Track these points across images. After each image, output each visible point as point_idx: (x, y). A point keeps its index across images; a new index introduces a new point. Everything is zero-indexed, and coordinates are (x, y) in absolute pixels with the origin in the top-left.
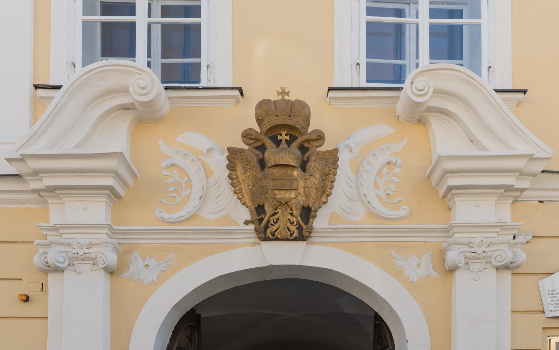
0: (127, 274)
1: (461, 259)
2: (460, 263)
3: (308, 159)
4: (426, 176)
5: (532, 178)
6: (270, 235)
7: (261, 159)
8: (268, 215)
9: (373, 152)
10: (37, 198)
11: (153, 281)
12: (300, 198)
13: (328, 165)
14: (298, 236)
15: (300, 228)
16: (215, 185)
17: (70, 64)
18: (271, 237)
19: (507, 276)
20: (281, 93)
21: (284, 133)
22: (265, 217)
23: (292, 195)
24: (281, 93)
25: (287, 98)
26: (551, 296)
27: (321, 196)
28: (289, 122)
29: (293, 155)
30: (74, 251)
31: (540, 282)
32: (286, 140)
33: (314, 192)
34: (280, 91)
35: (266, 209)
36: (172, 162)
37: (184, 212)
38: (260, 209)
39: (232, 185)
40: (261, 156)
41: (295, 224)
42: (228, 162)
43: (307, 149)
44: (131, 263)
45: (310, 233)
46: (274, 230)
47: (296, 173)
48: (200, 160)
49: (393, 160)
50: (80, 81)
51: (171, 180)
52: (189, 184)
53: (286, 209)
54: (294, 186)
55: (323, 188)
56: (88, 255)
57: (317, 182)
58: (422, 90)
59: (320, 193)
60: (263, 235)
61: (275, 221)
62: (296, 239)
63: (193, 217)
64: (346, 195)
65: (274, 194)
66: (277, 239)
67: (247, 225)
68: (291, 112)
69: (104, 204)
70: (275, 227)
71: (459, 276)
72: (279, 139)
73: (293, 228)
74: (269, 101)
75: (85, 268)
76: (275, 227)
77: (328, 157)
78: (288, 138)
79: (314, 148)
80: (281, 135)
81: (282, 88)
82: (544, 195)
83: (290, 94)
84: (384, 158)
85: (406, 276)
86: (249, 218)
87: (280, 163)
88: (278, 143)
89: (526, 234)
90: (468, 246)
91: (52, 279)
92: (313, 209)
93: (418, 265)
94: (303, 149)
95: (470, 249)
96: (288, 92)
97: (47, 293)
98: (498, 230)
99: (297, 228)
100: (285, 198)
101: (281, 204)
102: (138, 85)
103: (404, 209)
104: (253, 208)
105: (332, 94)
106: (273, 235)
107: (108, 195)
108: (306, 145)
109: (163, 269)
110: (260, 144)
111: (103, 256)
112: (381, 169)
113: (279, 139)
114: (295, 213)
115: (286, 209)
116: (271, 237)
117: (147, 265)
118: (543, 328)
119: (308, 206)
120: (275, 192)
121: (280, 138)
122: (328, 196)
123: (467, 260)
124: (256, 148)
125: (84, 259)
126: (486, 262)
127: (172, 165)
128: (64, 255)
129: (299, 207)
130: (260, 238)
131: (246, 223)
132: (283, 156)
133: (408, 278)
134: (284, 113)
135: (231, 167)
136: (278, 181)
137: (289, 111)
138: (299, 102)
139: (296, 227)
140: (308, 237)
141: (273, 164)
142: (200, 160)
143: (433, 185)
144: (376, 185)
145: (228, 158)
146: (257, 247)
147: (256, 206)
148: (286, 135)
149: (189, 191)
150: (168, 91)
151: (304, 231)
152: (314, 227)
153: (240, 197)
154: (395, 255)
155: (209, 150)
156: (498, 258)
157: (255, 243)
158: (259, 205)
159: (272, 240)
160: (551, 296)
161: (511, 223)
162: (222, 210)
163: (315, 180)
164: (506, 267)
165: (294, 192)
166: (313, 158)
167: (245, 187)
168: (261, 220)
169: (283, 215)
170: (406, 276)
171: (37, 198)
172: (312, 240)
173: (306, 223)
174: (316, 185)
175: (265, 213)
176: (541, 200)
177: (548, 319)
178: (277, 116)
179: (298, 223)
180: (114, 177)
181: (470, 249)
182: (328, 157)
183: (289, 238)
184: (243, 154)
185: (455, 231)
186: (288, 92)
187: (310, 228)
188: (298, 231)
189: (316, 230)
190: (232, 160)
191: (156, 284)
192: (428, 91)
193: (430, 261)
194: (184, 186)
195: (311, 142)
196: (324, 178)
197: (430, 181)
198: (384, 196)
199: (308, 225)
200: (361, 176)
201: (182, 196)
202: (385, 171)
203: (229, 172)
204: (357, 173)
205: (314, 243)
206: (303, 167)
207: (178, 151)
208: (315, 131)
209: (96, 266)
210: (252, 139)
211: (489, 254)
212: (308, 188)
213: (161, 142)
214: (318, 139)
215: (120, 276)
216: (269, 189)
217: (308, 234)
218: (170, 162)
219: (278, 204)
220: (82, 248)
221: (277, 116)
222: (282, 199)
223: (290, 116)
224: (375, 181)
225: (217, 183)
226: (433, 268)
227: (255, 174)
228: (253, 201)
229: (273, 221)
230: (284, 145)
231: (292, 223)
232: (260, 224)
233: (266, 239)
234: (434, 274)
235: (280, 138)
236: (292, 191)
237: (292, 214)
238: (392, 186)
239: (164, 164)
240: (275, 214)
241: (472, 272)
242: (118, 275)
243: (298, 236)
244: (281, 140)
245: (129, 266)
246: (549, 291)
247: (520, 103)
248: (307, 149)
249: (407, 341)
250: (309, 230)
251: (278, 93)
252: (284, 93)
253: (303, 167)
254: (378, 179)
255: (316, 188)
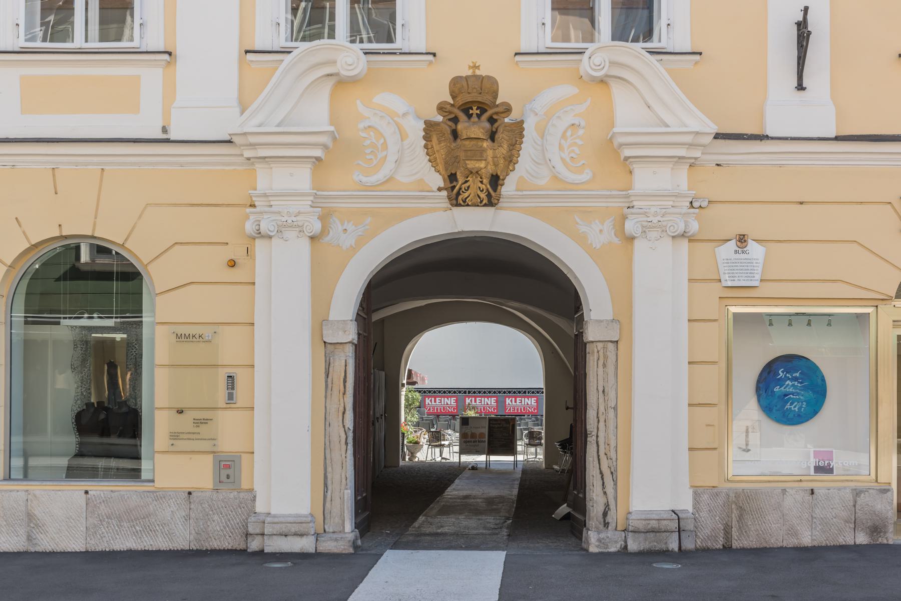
0: (327, 239)
1: (638, 229)
2: (636, 233)
3: (497, 129)
4: (608, 138)
5: (703, 148)
6: (461, 202)
7: (454, 129)
8: (460, 183)
9: (557, 115)
10: (244, 161)
11: (351, 246)
12: (489, 167)
13: (515, 135)
14: (487, 203)
15: (489, 196)
16: (409, 148)
17: (274, 23)
18: (463, 204)
19: (685, 244)
20: (472, 67)
21: (475, 108)
22: (457, 185)
23: (482, 165)
24: (472, 67)
25: (478, 72)
26: (725, 265)
27: (509, 165)
28: (479, 99)
29: (483, 130)
30: (284, 219)
31: (716, 249)
32: (477, 114)
33: (502, 161)
34: (471, 65)
35: (458, 177)
36: (370, 124)
37: (380, 176)
38: (452, 177)
39: (427, 154)
40: (454, 127)
41: (484, 191)
42: (424, 134)
43: (496, 121)
44: (330, 227)
45: (498, 200)
46: (465, 197)
47: (485, 144)
48: (395, 121)
49: (577, 123)
50: (295, 60)
51: (368, 142)
52: (385, 146)
53: (476, 177)
54: (483, 157)
55: (510, 158)
56: (295, 223)
57: (505, 152)
58: (599, 65)
59: (507, 163)
60: (454, 202)
61: (466, 188)
62: (485, 205)
63: (390, 180)
64: (533, 159)
65: (466, 164)
66: (468, 205)
67: (440, 191)
68: (481, 90)
69: (309, 170)
70: (466, 195)
71: (637, 243)
72: (470, 113)
73: (483, 195)
74: (461, 77)
75: (291, 234)
76: (466, 195)
77: (514, 128)
78: (478, 112)
79: (502, 119)
80: (472, 109)
81: (473, 62)
82: (721, 159)
83: (480, 67)
84: (568, 119)
85: (589, 242)
86: (442, 185)
87: (471, 137)
88: (470, 116)
89: (702, 200)
90: (644, 216)
91: (259, 243)
92: (501, 177)
93: (601, 231)
94: (492, 120)
95: (646, 219)
96: (479, 66)
97: (253, 259)
98: (673, 198)
99: (486, 195)
100: (475, 168)
101: (471, 173)
102: (346, 62)
103: (587, 173)
104: (446, 177)
105: (518, 58)
106: (464, 201)
107: (314, 162)
108: (495, 117)
109: (360, 233)
110: (452, 116)
111: (311, 226)
112: (565, 132)
113: (470, 113)
114: (485, 181)
115: (476, 177)
116: (463, 204)
117: (346, 229)
118: (720, 298)
119: (497, 175)
120: (467, 162)
121: (471, 112)
122: (515, 164)
123: (644, 229)
124: (450, 120)
125: (291, 227)
126: (663, 231)
127: (369, 127)
128: (274, 223)
129: (489, 175)
130: (452, 205)
131: (440, 189)
132: (474, 131)
133: (591, 244)
134: (475, 90)
135: (427, 138)
136: (469, 152)
137: (479, 89)
138: (489, 77)
139: (486, 194)
140: (496, 204)
141: (465, 138)
142: (395, 121)
143: (615, 147)
144: (561, 148)
145: (425, 130)
146: (449, 212)
147: (449, 174)
148: (477, 109)
149: (385, 153)
150: (367, 55)
151: (493, 198)
152: (502, 194)
153: (434, 166)
154: (578, 220)
155: (404, 115)
156: (672, 228)
157: (447, 208)
158: (451, 173)
159: (463, 206)
160: (725, 265)
161: (688, 191)
162: (416, 173)
163: (503, 150)
164: (683, 235)
165: (484, 162)
166: (501, 130)
167: (441, 155)
168: (453, 188)
169: (474, 183)
170: (589, 242)
171: (244, 161)
172: (500, 205)
173: (495, 190)
174: (504, 155)
175: (457, 180)
176: (718, 163)
177: (726, 289)
178: (469, 93)
179: (488, 190)
180: (322, 148)
181: (646, 219)
182: (514, 128)
183: (479, 204)
184: (439, 127)
185: (633, 199)
186: (479, 66)
187: (498, 196)
188: (487, 199)
189: (504, 196)
190: (428, 132)
191: (354, 249)
192: (605, 65)
193: (612, 226)
194: (380, 149)
195: (499, 114)
196: (511, 148)
197: (612, 143)
198: (568, 160)
199: (496, 193)
200: (547, 140)
201: (379, 159)
202: (569, 133)
203: (425, 142)
204: (542, 137)
205: (501, 209)
206: (492, 137)
207: (375, 113)
208: (503, 104)
209: (302, 233)
210: (446, 112)
211: (664, 224)
212: (496, 157)
213: (358, 102)
214: (505, 112)
215: (320, 241)
216: (461, 159)
217: (496, 202)
218: (367, 124)
219: (469, 173)
220: (290, 216)
221: (469, 93)
222: (473, 168)
223: (480, 93)
224: (560, 144)
225: (411, 146)
226: (615, 235)
227: (448, 145)
228: (446, 170)
229: (465, 188)
230: (474, 118)
231: (482, 191)
232: (452, 190)
233: (458, 205)
234: (616, 240)
235: (471, 112)
236: (483, 161)
237: (482, 182)
238: (575, 148)
239: (361, 126)
240: (466, 182)
241: (650, 240)
242: (319, 240)
243: (487, 203)
244: (472, 114)
245: (329, 230)
246: (724, 260)
247: (696, 63)
248: (496, 121)
249: (591, 310)
250: (497, 198)
251: (470, 67)
252: (475, 67)
253: (492, 137)
254: (563, 142)
255: (504, 158)
